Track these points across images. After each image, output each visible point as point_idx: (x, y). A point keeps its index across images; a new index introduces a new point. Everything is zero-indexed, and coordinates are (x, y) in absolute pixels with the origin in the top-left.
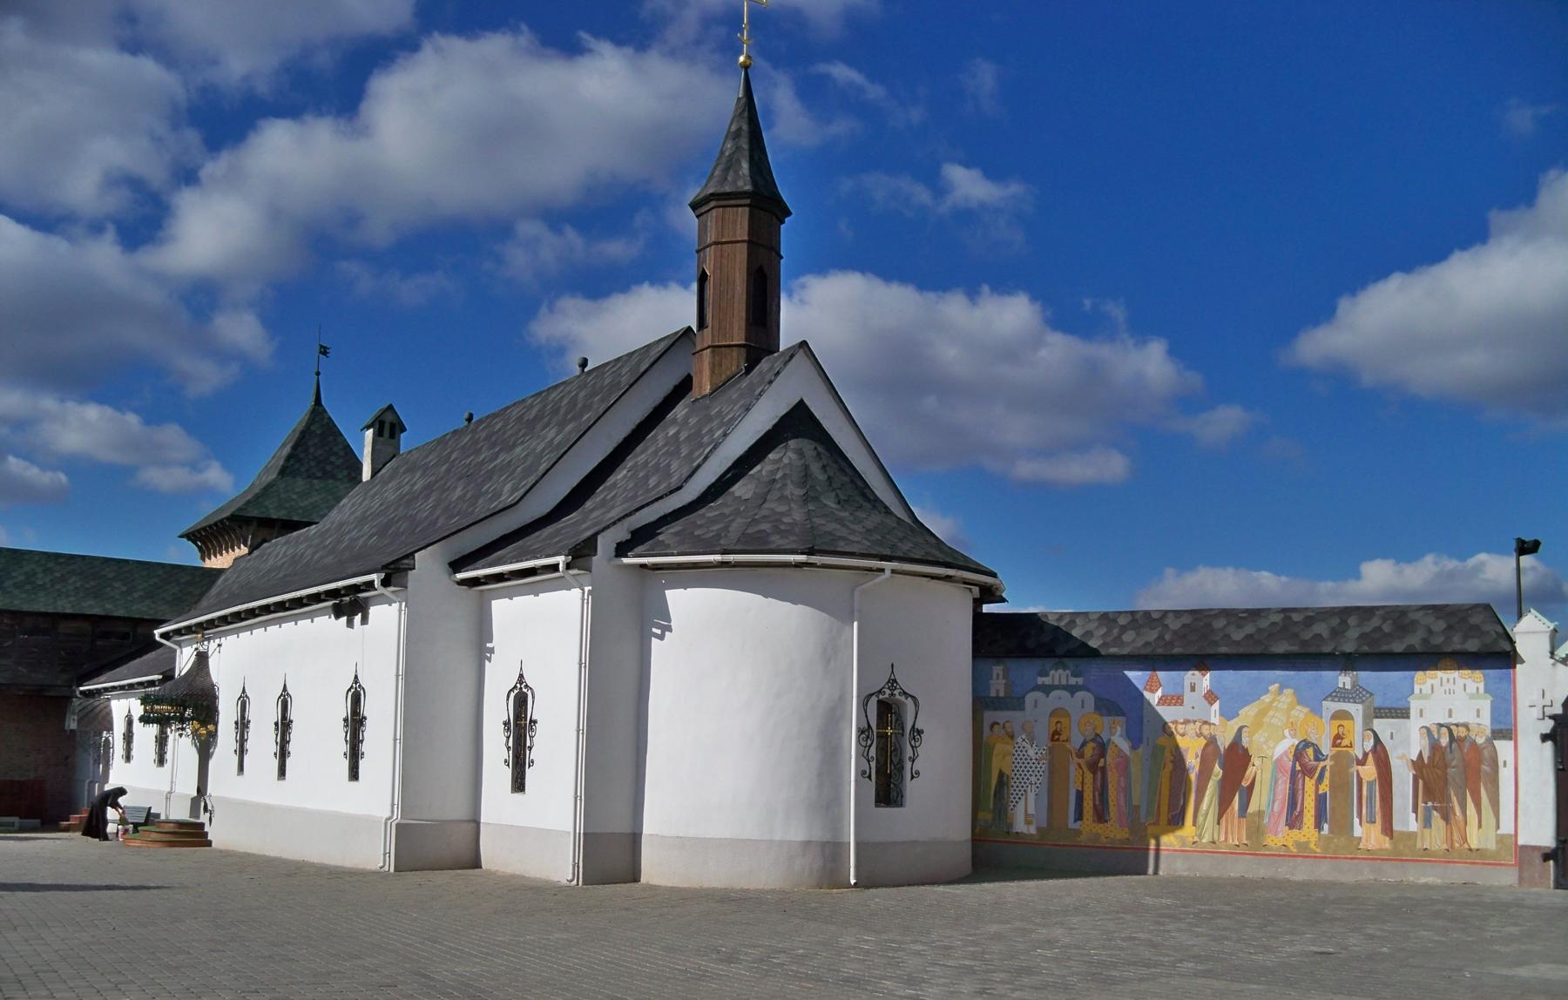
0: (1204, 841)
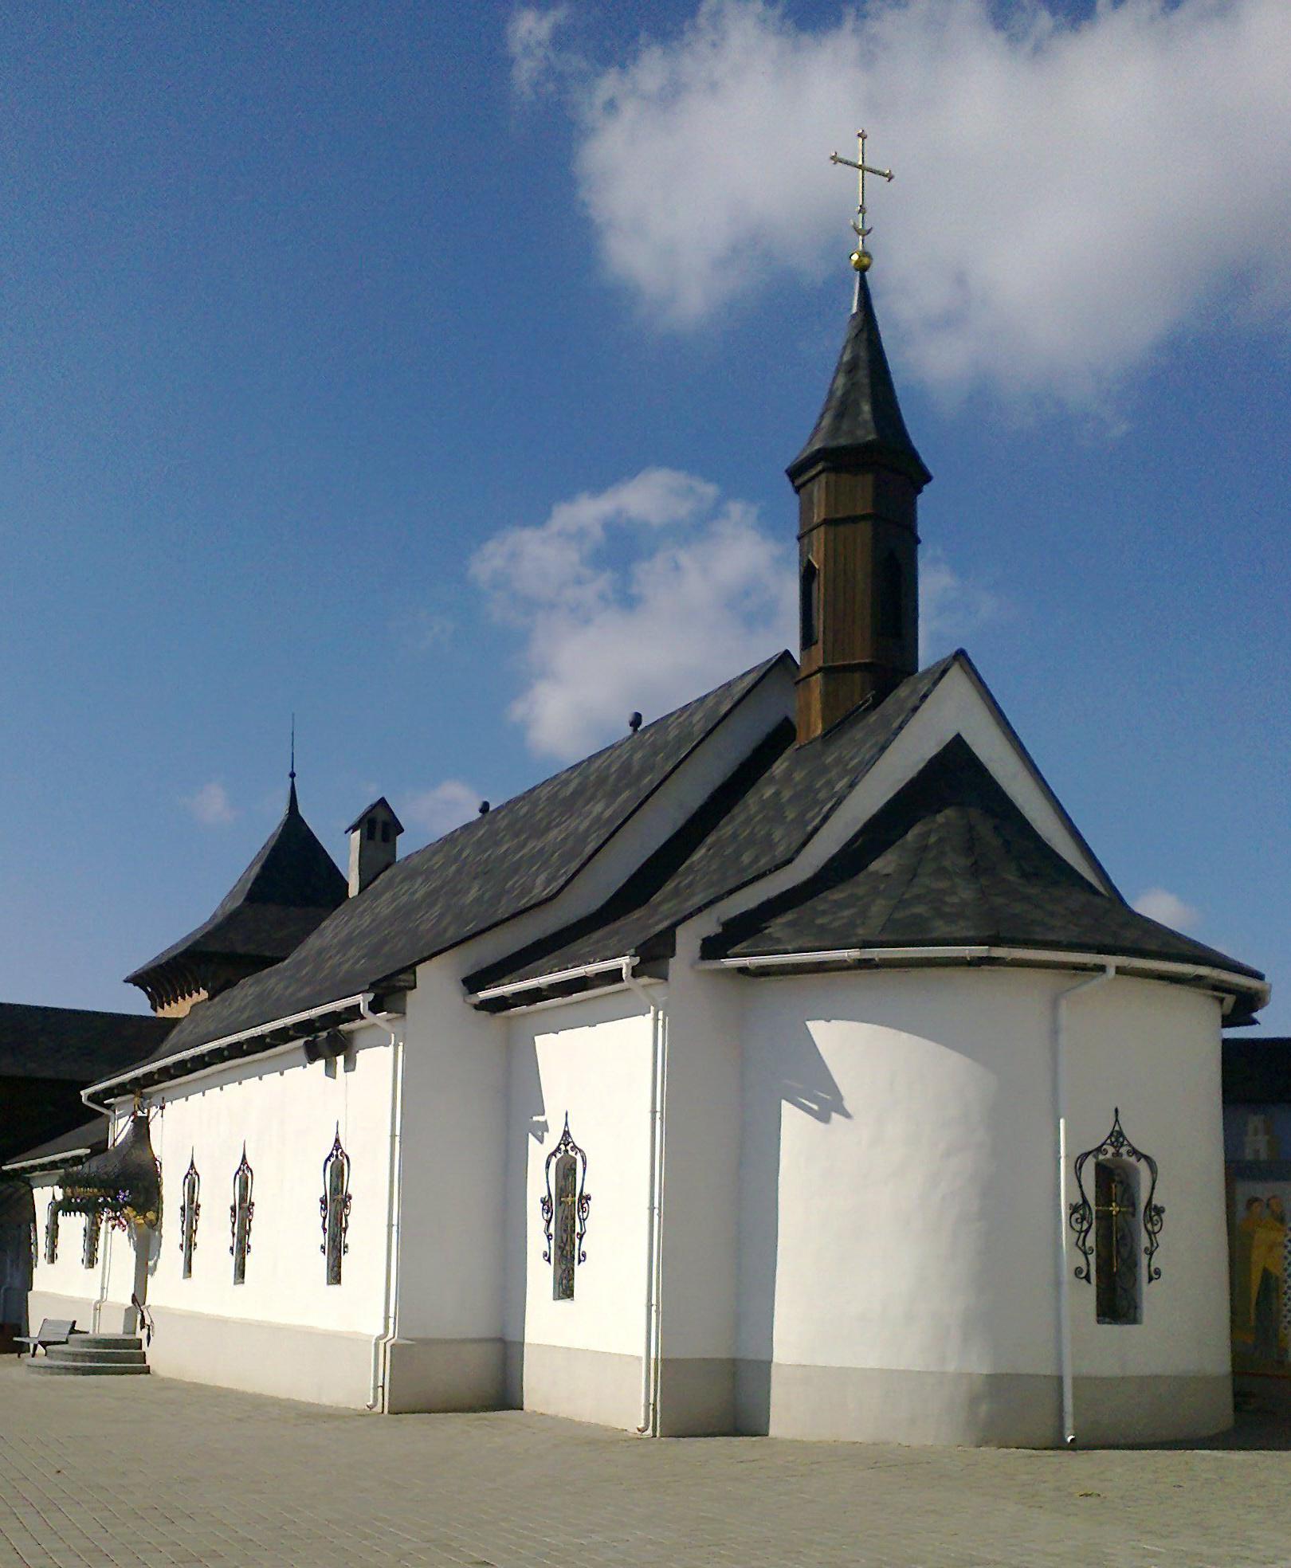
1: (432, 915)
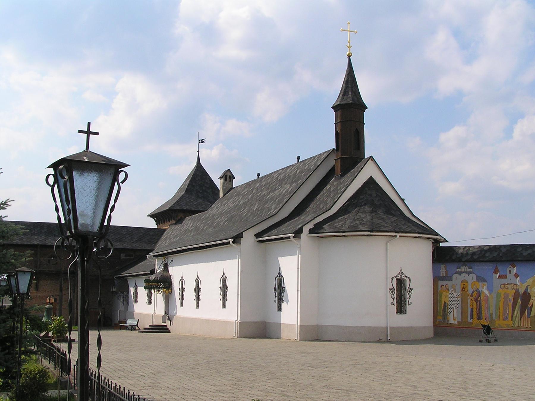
0: (516, 326)
1: (245, 211)
